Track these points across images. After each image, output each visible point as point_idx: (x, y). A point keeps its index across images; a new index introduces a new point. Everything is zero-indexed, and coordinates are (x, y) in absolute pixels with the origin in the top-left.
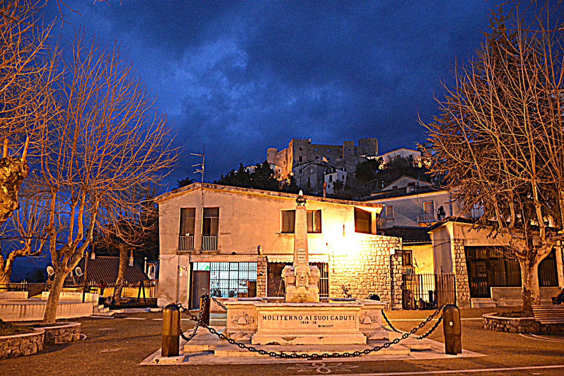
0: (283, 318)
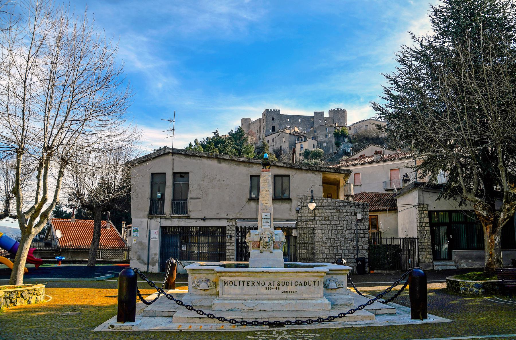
0: (245, 284)
